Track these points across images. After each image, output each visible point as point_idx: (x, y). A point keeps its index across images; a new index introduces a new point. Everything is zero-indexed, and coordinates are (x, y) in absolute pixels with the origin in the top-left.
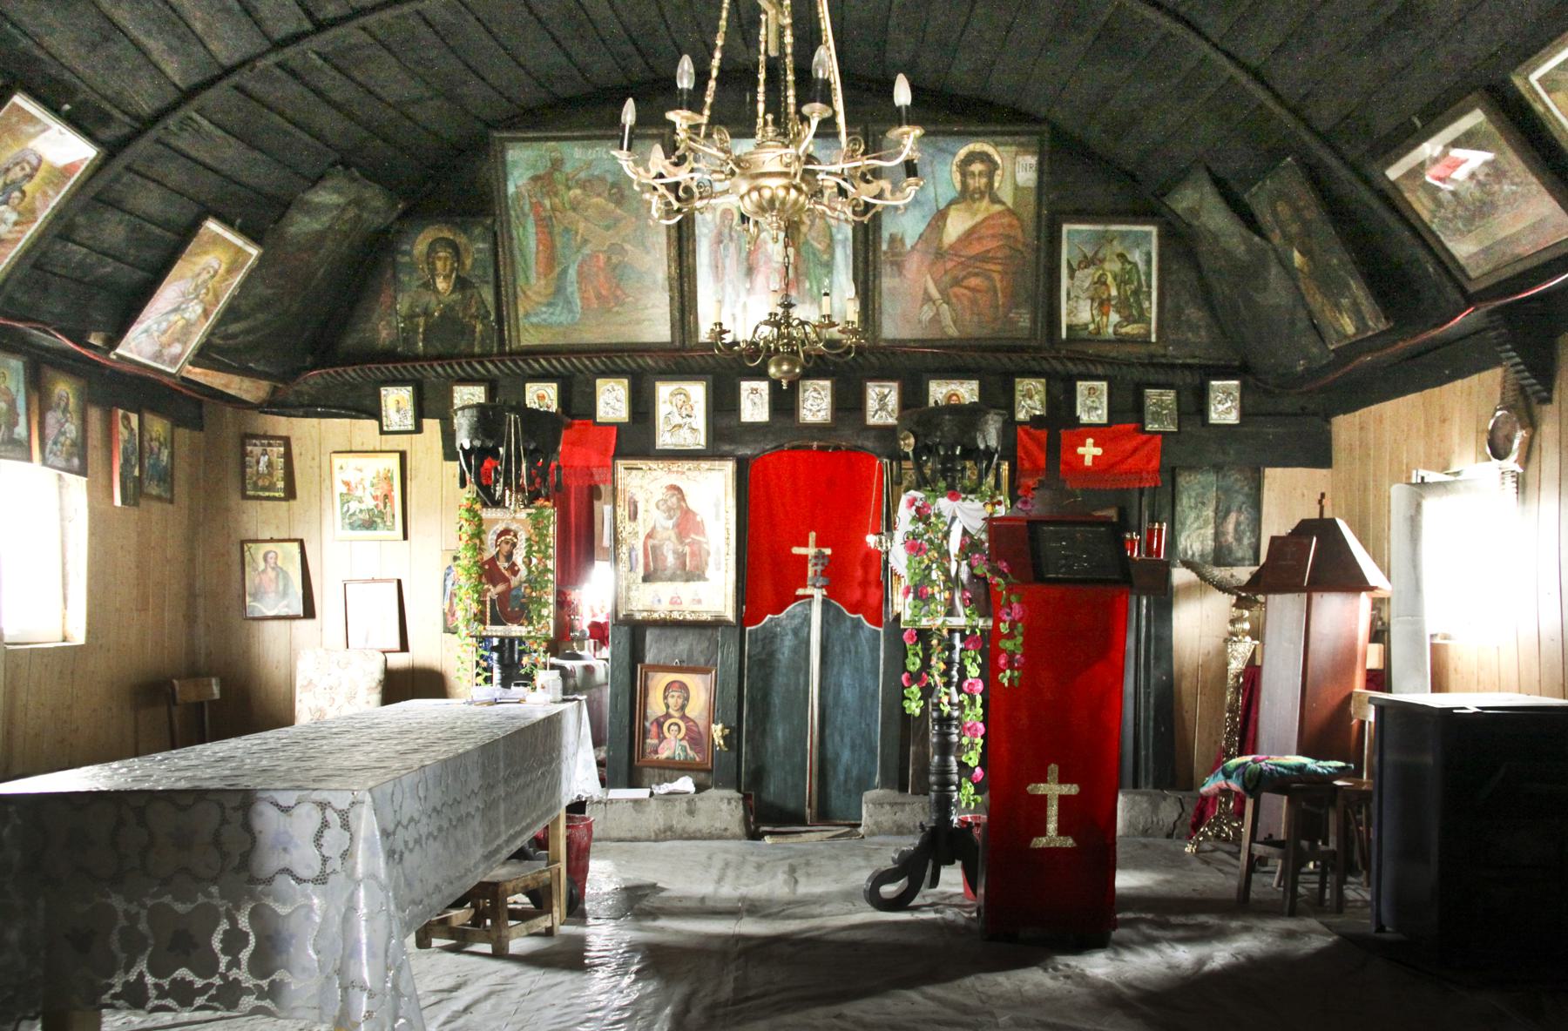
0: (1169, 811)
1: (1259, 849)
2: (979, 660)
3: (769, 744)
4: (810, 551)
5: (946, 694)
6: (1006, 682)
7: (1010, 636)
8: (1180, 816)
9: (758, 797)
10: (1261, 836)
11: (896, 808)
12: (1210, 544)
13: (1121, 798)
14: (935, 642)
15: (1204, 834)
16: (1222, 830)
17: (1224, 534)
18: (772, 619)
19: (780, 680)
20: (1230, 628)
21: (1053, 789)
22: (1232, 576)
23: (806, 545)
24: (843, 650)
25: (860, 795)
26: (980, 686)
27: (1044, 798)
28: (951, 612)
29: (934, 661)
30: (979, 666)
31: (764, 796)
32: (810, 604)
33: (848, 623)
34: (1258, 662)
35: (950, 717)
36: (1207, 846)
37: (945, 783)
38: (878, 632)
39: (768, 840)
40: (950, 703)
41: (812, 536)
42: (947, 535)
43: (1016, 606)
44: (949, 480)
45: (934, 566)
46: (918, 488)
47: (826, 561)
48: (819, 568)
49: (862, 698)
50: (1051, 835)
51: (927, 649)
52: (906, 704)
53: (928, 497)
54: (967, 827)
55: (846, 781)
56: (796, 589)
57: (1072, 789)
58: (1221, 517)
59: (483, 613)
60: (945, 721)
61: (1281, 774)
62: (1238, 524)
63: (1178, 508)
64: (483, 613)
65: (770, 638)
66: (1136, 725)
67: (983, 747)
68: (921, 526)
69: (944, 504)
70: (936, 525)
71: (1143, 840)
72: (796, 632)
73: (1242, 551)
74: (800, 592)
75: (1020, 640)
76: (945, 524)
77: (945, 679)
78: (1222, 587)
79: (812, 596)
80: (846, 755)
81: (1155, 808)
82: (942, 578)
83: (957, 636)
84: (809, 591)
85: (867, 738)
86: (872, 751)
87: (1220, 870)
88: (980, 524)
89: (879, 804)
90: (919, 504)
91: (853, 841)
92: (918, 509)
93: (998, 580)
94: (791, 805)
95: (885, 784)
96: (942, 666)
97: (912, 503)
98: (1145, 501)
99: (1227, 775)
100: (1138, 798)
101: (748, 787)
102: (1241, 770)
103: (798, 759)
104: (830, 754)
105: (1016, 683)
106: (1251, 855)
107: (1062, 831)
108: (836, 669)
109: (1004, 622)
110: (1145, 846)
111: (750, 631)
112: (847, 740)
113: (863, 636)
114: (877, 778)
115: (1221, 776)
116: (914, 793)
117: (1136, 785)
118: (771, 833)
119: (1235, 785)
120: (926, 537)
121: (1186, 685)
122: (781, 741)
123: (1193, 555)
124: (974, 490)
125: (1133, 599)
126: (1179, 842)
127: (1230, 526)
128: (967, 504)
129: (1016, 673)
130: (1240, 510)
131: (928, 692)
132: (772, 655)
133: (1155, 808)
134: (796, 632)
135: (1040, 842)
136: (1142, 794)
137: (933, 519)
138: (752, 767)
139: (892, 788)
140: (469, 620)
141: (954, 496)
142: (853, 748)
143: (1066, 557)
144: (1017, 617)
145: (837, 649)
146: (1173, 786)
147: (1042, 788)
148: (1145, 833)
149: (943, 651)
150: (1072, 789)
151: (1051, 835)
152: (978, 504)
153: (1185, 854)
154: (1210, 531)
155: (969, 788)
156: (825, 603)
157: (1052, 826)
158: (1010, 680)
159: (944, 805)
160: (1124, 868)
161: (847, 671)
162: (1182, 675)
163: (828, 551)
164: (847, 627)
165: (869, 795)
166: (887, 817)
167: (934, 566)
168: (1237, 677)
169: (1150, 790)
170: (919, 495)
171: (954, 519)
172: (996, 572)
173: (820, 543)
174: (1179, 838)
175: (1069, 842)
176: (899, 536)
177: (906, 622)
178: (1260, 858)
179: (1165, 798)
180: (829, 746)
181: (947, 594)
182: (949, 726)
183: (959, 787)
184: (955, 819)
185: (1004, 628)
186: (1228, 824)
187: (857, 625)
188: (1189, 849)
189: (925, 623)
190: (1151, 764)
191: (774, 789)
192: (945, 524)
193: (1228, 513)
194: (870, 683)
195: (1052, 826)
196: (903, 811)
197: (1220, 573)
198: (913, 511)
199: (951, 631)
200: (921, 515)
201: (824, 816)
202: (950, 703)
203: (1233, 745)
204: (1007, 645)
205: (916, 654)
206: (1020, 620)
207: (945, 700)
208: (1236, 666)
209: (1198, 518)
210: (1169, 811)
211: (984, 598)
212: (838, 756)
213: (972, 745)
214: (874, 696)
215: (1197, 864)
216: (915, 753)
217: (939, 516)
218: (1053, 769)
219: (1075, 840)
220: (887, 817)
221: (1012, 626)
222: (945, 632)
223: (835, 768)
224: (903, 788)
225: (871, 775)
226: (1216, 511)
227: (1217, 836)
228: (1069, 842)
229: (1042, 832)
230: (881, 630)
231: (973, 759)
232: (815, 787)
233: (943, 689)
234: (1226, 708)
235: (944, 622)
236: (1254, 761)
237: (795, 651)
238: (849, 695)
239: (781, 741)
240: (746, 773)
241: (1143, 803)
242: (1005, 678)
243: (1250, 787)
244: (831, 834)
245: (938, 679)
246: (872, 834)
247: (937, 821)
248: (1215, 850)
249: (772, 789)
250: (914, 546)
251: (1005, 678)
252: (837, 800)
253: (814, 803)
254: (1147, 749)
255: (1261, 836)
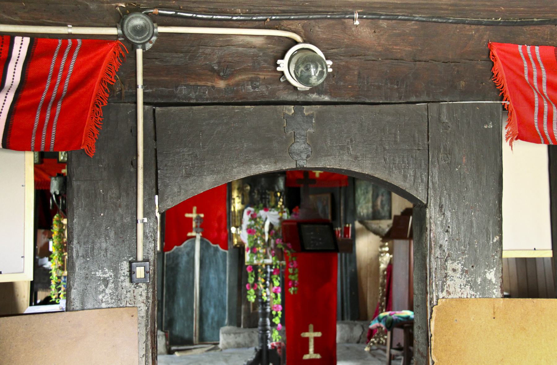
0: (358, 332)
1: (394, 352)
2: (279, 279)
3: (176, 306)
4: (194, 215)
5: (265, 292)
6: (292, 293)
7: (293, 274)
8: (362, 333)
9: (171, 334)
10: (395, 346)
11: (237, 335)
12: (371, 210)
13: (338, 327)
14: (259, 270)
15: (373, 342)
16: (380, 340)
17: (377, 205)
18: (177, 248)
19: (181, 277)
20: (380, 250)
21: (311, 335)
22: (380, 227)
23: (191, 212)
24: (210, 262)
25: (218, 329)
26: (280, 290)
27: (307, 339)
28: (266, 257)
29: (260, 279)
30: (279, 281)
31: (174, 332)
32: (194, 241)
33: (212, 249)
34: (392, 263)
35: (267, 302)
36: (374, 347)
37: (265, 330)
38: (225, 253)
39: (177, 354)
40: (267, 296)
41: (195, 209)
42: (263, 226)
43: (295, 262)
44: (264, 202)
45: (259, 238)
46: (251, 206)
47: (202, 221)
48: (199, 224)
49: (219, 284)
50: (311, 354)
51: (257, 274)
52: (248, 297)
53: (255, 211)
54: (274, 348)
55: (212, 323)
56: (187, 233)
57: (319, 334)
58: (375, 197)
59: (63, 265)
60: (265, 304)
61: (400, 321)
62: (382, 201)
63: (357, 195)
64: (63, 265)
65: (176, 257)
66: (342, 299)
67: (282, 315)
68: (253, 222)
69: (262, 213)
70: (259, 222)
71: (347, 345)
72: (188, 254)
73: (384, 213)
74: (189, 234)
75: (297, 275)
76: (262, 221)
77: (264, 286)
78: (376, 233)
79: (195, 237)
80: (212, 311)
81: (352, 329)
82: (262, 244)
83: (269, 267)
84: (194, 234)
85: (221, 301)
86: (224, 308)
87: (380, 360)
88: (277, 221)
89: (228, 333)
90: (252, 213)
91: (217, 352)
92: (252, 215)
93: (287, 251)
94: (187, 336)
95: (230, 324)
96: (263, 280)
97: (249, 212)
98: (342, 191)
99: (380, 321)
100: (344, 325)
101: (166, 329)
102: (385, 319)
103: (190, 313)
104: (204, 310)
105: (296, 293)
106: (390, 355)
107: (315, 352)
108: (206, 271)
109: (290, 268)
110: (348, 348)
111: (167, 255)
112: (212, 303)
113: (219, 255)
114: (226, 321)
115: (377, 321)
116: (244, 327)
117: (343, 319)
118: (178, 351)
119: (382, 325)
120: (255, 227)
121: (363, 273)
122: (181, 306)
123: (364, 215)
124: (275, 207)
125: (339, 255)
126: (363, 345)
127: (379, 202)
128: (272, 213)
129: (296, 289)
130: (382, 195)
131: (257, 291)
132: (177, 265)
133: (352, 329)
134: (188, 254)
135: (306, 357)
136: (346, 323)
137: (258, 220)
138: (168, 318)
139: (234, 325)
140: (57, 269)
141: (266, 210)
142: (215, 307)
143: (313, 240)
144: (296, 266)
145: (207, 261)
146: (359, 319)
147: (306, 335)
148: (348, 341)
149: (263, 274)
150: (319, 334)
151: (311, 354)
152: (276, 213)
153: (365, 352)
154: (370, 205)
155: (276, 333)
156: (202, 241)
157: (311, 350)
158: (294, 291)
159: (264, 339)
160: (340, 360)
161: (212, 271)
162: (361, 269)
163: (202, 215)
164: (211, 251)
165: (223, 329)
166: (232, 339)
167: (259, 238)
168: (384, 271)
169: (349, 321)
170: (252, 209)
171: (266, 219)
172: (287, 248)
173: (198, 212)
174: (363, 343)
175: (318, 356)
176: (244, 226)
177: (247, 262)
178: (394, 356)
179: (355, 325)
180: (204, 306)
181: (264, 251)
182: (266, 305)
183: (272, 332)
184: (269, 346)
185: (290, 271)
186: (383, 337)
187: (216, 250)
188: (367, 349)
189: (255, 262)
190: (349, 309)
191: (178, 328)
192: (262, 221)
193: (377, 196)
194: (222, 276)
195: (311, 350)
196: (239, 336)
197: (374, 224)
198: (250, 216)
199: (266, 265)
200: (253, 217)
201: (202, 340)
202: (267, 296)
203: (383, 301)
204: (292, 278)
205: (252, 276)
206: (297, 267)
207: (264, 294)
208: (383, 266)
209: (365, 199)
210: (358, 332)
211: (279, 254)
212: (208, 311)
213: (277, 315)
214: (224, 282)
215: (370, 357)
216: (245, 309)
217: (260, 218)
218: (311, 326)
219: (321, 355)
220: (232, 339)
221: (294, 270)
222: (264, 266)
223: (207, 317)
224: (239, 325)
225: (224, 319)
226: (373, 195)
227: (378, 343)
228: (318, 356)
229: (307, 352)
230: (227, 251)
231: (277, 321)
232: (197, 327)
233: (264, 290)
234: (380, 285)
235: (263, 262)
236: (390, 315)
237: (188, 263)
238: (213, 283)
239: (181, 306)
240: (165, 322)
241: (346, 327)
242: (292, 290)
243: (388, 326)
244: (206, 349)
245: (261, 286)
246: (226, 348)
247: (262, 347)
248: (378, 349)
249: (177, 328)
250: (250, 231)
251: (292, 290)
252: (208, 333)
253: (197, 335)
254: (347, 303)
255: (395, 346)
